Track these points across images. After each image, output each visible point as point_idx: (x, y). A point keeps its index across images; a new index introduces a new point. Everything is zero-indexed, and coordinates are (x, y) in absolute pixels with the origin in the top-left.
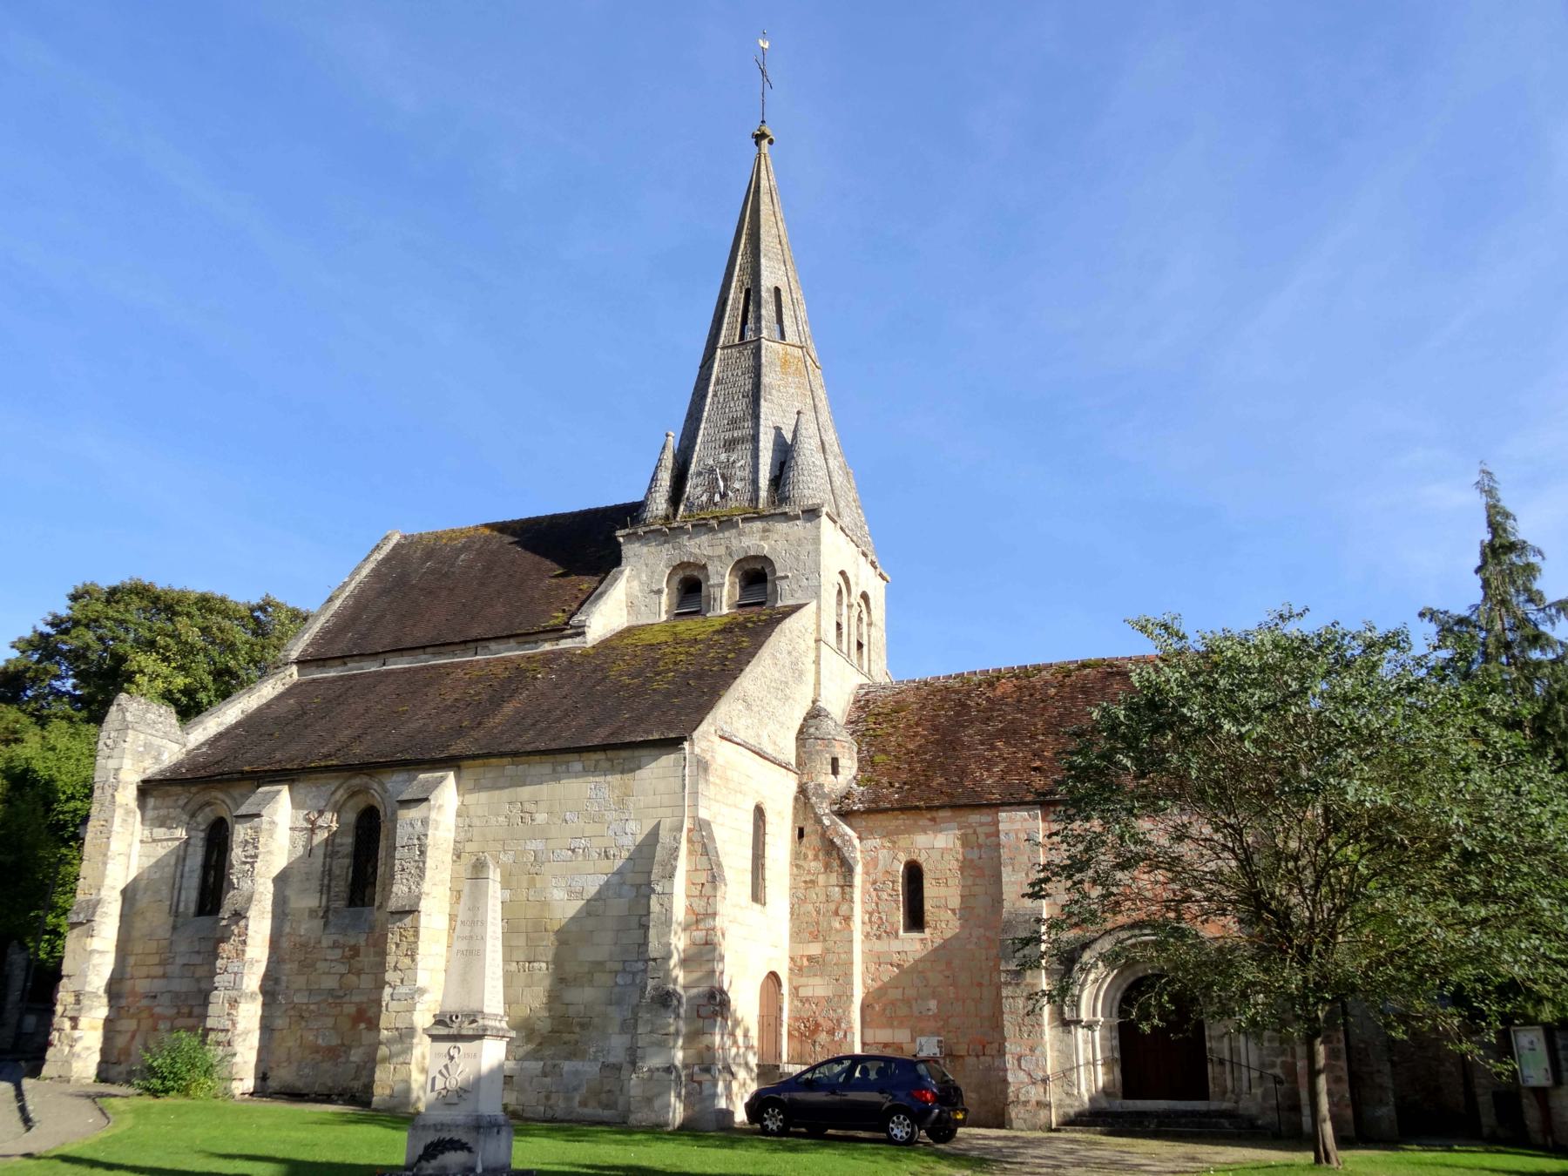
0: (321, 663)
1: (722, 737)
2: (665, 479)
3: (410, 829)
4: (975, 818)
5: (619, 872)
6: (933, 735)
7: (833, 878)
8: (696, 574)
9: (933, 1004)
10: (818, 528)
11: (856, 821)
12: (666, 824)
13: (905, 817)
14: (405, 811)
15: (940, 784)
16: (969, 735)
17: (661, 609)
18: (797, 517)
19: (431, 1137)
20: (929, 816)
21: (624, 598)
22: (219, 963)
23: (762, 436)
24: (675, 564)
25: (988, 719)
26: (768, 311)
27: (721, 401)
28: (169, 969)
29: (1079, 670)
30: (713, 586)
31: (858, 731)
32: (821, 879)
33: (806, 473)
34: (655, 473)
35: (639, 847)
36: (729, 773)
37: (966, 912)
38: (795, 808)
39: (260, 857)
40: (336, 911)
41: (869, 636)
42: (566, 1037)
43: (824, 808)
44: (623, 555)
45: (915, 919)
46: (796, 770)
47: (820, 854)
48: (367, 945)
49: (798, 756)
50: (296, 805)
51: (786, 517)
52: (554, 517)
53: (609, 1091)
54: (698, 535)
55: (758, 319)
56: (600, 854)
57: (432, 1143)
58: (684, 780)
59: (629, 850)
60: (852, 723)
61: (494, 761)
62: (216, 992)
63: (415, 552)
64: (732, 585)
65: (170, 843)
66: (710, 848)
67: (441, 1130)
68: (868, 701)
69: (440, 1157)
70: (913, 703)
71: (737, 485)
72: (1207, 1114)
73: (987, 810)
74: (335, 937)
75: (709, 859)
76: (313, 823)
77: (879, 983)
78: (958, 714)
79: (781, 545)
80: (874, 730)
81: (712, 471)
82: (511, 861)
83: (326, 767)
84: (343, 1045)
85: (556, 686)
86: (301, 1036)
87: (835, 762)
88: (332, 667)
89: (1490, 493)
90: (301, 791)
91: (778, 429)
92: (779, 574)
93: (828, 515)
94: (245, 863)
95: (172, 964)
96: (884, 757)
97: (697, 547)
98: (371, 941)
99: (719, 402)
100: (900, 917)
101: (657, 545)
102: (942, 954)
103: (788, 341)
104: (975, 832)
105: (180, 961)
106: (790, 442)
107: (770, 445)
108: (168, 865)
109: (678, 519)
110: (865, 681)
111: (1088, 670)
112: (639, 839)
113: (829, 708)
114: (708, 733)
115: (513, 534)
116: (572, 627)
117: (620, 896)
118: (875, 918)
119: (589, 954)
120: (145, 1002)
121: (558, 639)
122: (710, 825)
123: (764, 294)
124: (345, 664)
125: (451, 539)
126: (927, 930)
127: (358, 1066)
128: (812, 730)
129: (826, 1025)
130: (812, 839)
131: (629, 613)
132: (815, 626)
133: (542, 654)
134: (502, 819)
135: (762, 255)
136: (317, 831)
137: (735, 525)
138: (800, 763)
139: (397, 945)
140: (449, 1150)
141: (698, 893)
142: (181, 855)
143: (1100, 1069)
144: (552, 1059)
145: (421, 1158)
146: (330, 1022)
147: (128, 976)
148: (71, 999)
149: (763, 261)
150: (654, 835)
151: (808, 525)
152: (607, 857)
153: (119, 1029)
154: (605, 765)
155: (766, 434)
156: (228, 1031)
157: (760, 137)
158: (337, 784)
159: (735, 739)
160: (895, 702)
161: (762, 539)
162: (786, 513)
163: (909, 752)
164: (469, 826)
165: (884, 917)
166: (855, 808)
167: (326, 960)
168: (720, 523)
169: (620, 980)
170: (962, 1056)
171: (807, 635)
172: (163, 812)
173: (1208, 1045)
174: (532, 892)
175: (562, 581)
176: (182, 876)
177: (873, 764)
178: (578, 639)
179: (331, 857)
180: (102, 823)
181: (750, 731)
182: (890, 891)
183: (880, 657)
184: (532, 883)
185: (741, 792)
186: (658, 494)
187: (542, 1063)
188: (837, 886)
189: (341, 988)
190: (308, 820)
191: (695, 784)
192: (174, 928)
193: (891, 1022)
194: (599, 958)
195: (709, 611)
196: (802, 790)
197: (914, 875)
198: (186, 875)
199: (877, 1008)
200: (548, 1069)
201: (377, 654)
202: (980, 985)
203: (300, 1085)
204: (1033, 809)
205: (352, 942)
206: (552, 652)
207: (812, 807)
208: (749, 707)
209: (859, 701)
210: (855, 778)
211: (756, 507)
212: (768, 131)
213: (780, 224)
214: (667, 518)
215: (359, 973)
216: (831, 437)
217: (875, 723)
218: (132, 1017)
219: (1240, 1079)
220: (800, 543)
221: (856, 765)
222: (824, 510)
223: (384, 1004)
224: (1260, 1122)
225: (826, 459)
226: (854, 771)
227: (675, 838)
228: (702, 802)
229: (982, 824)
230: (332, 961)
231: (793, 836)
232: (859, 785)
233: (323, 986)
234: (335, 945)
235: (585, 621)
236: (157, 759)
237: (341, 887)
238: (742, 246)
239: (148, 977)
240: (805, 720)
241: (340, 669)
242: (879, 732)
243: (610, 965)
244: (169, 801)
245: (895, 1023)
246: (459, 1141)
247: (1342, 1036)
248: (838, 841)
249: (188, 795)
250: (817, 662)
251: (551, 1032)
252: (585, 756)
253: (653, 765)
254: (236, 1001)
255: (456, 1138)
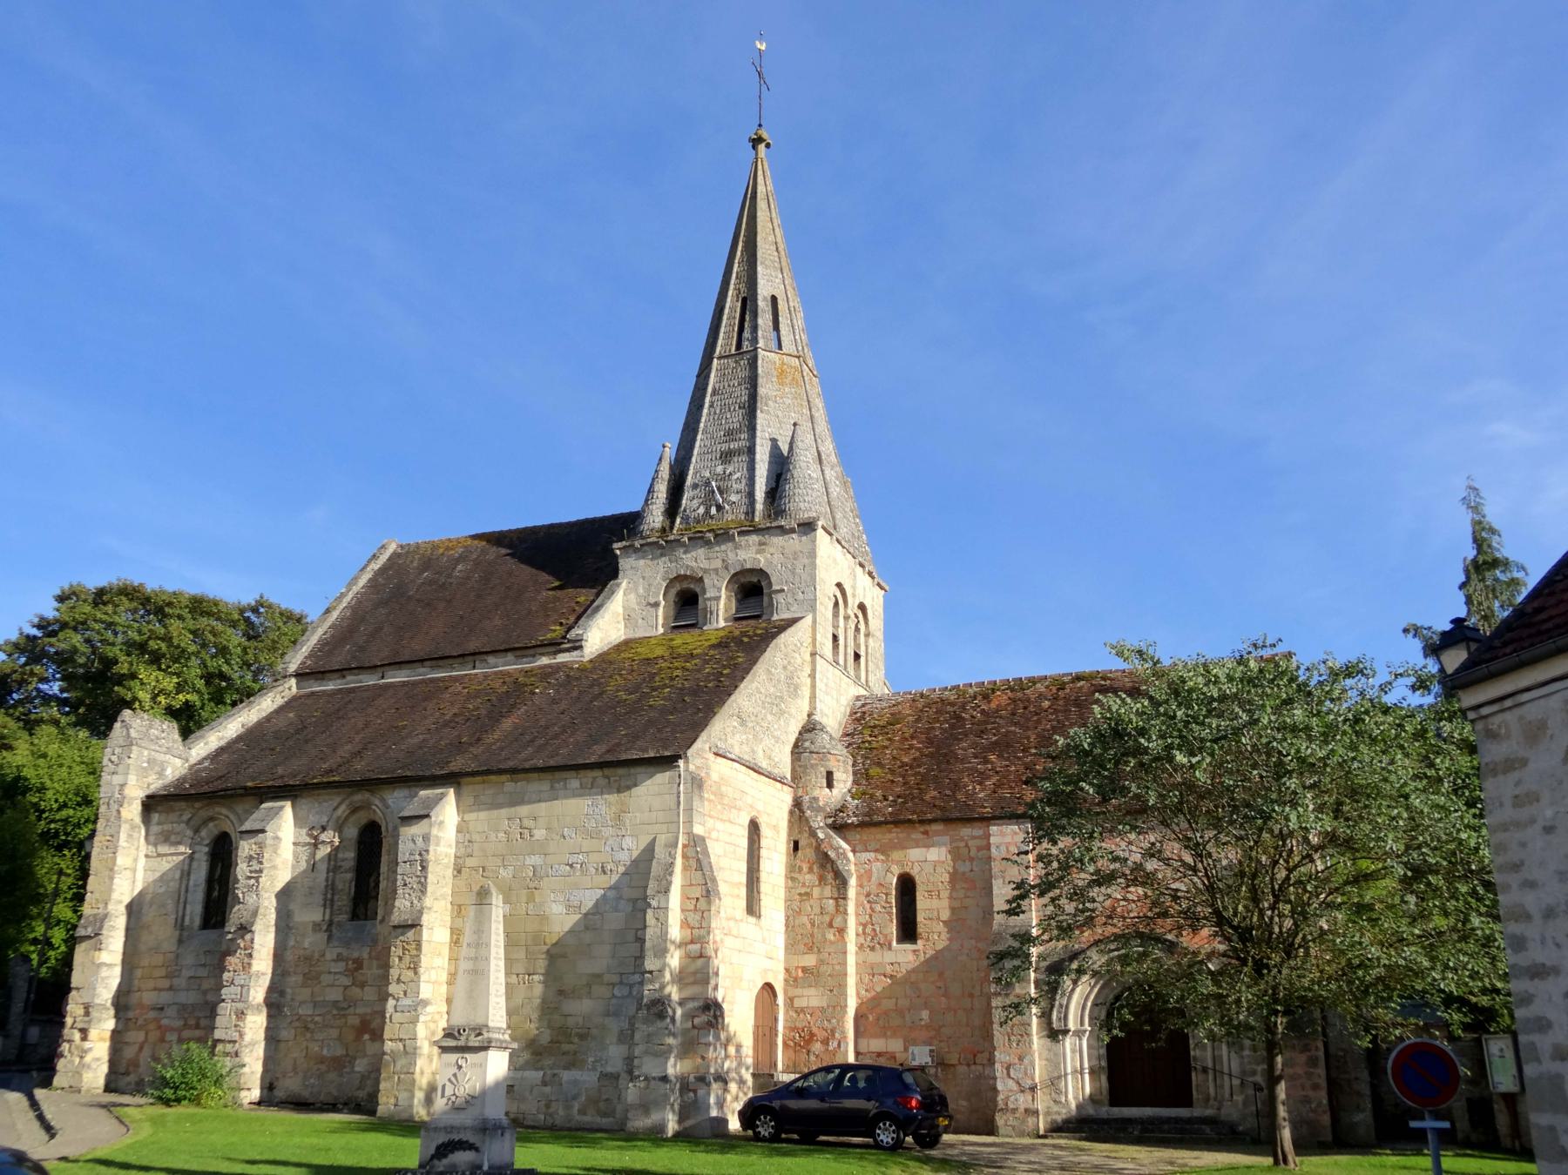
0: (320, 676)
1: (717, 754)
2: (662, 490)
3: (412, 845)
4: (966, 831)
5: (614, 887)
6: (927, 748)
7: (828, 891)
8: (692, 586)
9: (925, 1014)
10: (814, 541)
11: (851, 835)
12: (662, 840)
13: (898, 830)
14: (407, 828)
15: (934, 798)
16: (963, 748)
17: (657, 623)
18: (792, 531)
19: (442, 1138)
20: (922, 829)
21: (621, 610)
22: (226, 976)
23: (758, 449)
24: (671, 577)
25: (982, 732)
26: (765, 320)
27: (718, 412)
28: (176, 981)
29: (1073, 682)
30: (709, 599)
31: (854, 743)
32: (816, 892)
33: (801, 485)
34: (652, 485)
35: (635, 862)
36: (723, 789)
37: (955, 925)
38: (790, 821)
39: (265, 872)
40: (339, 924)
41: (867, 646)
42: (565, 1047)
43: (818, 822)
44: (620, 568)
45: (908, 931)
46: (792, 784)
47: (815, 867)
48: (370, 958)
49: (793, 770)
50: (298, 821)
51: (783, 531)
52: (552, 526)
53: (607, 1100)
54: (695, 548)
55: (755, 328)
56: (597, 869)
57: (443, 1144)
58: (679, 797)
59: (625, 865)
60: (848, 735)
61: (493, 777)
62: (222, 1004)
63: (412, 562)
64: (728, 598)
65: (175, 858)
66: (705, 863)
67: (451, 1132)
68: (864, 713)
69: (451, 1156)
70: (909, 715)
71: (734, 498)
72: (1190, 1121)
73: (979, 824)
74: (339, 950)
75: (704, 874)
76: (316, 838)
77: (873, 993)
78: (952, 727)
79: (777, 558)
80: (869, 742)
81: (708, 483)
82: (511, 876)
83: (329, 783)
84: (347, 1055)
85: (554, 701)
86: (307, 1048)
87: (829, 775)
88: (330, 680)
89: (1476, 509)
90: (304, 807)
91: (774, 441)
92: (775, 587)
93: (823, 528)
94: (250, 878)
95: (178, 976)
96: (879, 770)
97: (695, 560)
98: (373, 954)
99: (715, 413)
100: (893, 929)
101: (652, 559)
102: (934, 965)
103: (784, 351)
104: (967, 846)
105: (186, 973)
106: (786, 454)
107: (766, 457)
108: (173, 879)
109: (675, 532)
110: (864, 693)
111: (1082, 683)
112: (635, 854)
113: (824, 721)
114: (702, 750)
115: (509, 547)
116: (569, 641)
117: (616, 910)
118: (869, 930)
119: (587, 967)
120: (152, 1014)
121: (556, 653)
122: (704, 840)
123: (761, 303)
124: (344, 677)
125: (448, 549)
126: (919, 942)
127: (363, 1076)
128: (807, 744)
129: (821, 1035)
130: (807, 852)
131: (626, 627)
132: (810, 640)
133: (541, 667)
134: (501, 835)
135: (758, 263)
136: (320, 846)
137: (731, 539)
138: (795, 777)
139: (400, 959)
140: (458, 1149)
141: (692, 908)
142: (186, 872)
143: (1087, 1077)
144: (551, 1069)
145: (433, 1157)
146: (334, 1033)
147: (136, 989)
148: (80, 1011)
149: (759, 269)
150: (650, 850)
151: (804, 538)
152: (604, 873)
153: (127, 1040)
154: (602, 782)
155: (762, 446)
156: (235, 1042)
157: (756, 141)
158: (338, 800)
159: (730, 756)
160: (892, 714)
161: (758, 552)
162: (781, 527)
163: (903, 765)
164: (469, 841)
165: (878, 929)
166: (850, 821)
167: (330, 973)
168: (716, 536)
169: (616, 992)
170: (953, 1065)
171: (803, 649)
172: (166, 827)
173: (1192, 1053)
174: (531, 906)
175: (559, 593)
176: (187, 891)
177: (868, 777)
178: (575, 653)
179: (334, 872)
180: (108, 838)
181: (744, 746)
182: (883, 904)
183: (878, 667)
184: (531, 899)
185: (735, 807)
186: (654, 507)
187: (542, 1073)
188: (831, 898)
189: (345, 1000)
190: (310, 835)
191: (690, 801)
192: (180, 941)
193: (883, 1033)
194: (597, 970)
195: (705, 624)
196: (797, 804)
197: (907, 887)
198: (191, 889)
199: (871, 1018)
200: (547, 1079)
201: (338, 670)
202: (971, 995)
203: (306, 1095)
204: (1023, 823)
205: (356, 955)
206: (549, 666)
207: (807, 820)
208: (743, 723)
209: (856, 713)
210: (849, 791)
211: (753, 520)
212: (765, 135)
213: (777, 230)
214: (663, 530)
215: (362, 985)
216: (828, 447)
217: (870, 736)
218: (140, 1028)
219: (1222, 1086)
220: (795, 556)
221: (851, 779)
222: (820, 523)
223: (388, 1015)
224: (1241, 1128)
225: (822, 471)
226: (849, 784)
227: (670, 853)
228: (696, 818)
229: (974, 838)
230: (335, 973)
231: (788, 848)
232: (853, 798)
233: (327, 999)
234: (339, 958)
235: (582, 635)
236: (161, 774)
237: (344, 901)
238: (739, 253)
239: (155, 989)
240: (800, 733)
241: (339, 681)
242: (874, 745)
243: (607, 978)
244: (173, 816)
245: (889, 1033)
246: (467, 1142)
247: (1320, 1045)
248: (832, 854)
249: (191, 810)
250: (813, 676)
251: (551, 1042)
252: (582, 773)
253: (649, 782)
254: (243, 1013)
255: (465, 1139)
